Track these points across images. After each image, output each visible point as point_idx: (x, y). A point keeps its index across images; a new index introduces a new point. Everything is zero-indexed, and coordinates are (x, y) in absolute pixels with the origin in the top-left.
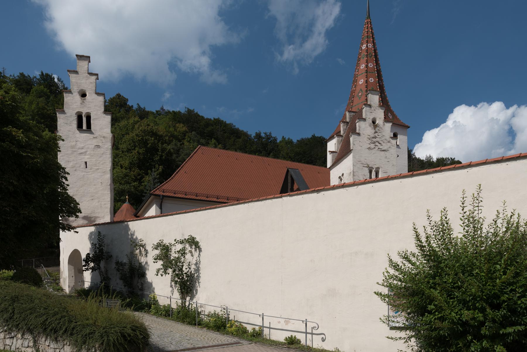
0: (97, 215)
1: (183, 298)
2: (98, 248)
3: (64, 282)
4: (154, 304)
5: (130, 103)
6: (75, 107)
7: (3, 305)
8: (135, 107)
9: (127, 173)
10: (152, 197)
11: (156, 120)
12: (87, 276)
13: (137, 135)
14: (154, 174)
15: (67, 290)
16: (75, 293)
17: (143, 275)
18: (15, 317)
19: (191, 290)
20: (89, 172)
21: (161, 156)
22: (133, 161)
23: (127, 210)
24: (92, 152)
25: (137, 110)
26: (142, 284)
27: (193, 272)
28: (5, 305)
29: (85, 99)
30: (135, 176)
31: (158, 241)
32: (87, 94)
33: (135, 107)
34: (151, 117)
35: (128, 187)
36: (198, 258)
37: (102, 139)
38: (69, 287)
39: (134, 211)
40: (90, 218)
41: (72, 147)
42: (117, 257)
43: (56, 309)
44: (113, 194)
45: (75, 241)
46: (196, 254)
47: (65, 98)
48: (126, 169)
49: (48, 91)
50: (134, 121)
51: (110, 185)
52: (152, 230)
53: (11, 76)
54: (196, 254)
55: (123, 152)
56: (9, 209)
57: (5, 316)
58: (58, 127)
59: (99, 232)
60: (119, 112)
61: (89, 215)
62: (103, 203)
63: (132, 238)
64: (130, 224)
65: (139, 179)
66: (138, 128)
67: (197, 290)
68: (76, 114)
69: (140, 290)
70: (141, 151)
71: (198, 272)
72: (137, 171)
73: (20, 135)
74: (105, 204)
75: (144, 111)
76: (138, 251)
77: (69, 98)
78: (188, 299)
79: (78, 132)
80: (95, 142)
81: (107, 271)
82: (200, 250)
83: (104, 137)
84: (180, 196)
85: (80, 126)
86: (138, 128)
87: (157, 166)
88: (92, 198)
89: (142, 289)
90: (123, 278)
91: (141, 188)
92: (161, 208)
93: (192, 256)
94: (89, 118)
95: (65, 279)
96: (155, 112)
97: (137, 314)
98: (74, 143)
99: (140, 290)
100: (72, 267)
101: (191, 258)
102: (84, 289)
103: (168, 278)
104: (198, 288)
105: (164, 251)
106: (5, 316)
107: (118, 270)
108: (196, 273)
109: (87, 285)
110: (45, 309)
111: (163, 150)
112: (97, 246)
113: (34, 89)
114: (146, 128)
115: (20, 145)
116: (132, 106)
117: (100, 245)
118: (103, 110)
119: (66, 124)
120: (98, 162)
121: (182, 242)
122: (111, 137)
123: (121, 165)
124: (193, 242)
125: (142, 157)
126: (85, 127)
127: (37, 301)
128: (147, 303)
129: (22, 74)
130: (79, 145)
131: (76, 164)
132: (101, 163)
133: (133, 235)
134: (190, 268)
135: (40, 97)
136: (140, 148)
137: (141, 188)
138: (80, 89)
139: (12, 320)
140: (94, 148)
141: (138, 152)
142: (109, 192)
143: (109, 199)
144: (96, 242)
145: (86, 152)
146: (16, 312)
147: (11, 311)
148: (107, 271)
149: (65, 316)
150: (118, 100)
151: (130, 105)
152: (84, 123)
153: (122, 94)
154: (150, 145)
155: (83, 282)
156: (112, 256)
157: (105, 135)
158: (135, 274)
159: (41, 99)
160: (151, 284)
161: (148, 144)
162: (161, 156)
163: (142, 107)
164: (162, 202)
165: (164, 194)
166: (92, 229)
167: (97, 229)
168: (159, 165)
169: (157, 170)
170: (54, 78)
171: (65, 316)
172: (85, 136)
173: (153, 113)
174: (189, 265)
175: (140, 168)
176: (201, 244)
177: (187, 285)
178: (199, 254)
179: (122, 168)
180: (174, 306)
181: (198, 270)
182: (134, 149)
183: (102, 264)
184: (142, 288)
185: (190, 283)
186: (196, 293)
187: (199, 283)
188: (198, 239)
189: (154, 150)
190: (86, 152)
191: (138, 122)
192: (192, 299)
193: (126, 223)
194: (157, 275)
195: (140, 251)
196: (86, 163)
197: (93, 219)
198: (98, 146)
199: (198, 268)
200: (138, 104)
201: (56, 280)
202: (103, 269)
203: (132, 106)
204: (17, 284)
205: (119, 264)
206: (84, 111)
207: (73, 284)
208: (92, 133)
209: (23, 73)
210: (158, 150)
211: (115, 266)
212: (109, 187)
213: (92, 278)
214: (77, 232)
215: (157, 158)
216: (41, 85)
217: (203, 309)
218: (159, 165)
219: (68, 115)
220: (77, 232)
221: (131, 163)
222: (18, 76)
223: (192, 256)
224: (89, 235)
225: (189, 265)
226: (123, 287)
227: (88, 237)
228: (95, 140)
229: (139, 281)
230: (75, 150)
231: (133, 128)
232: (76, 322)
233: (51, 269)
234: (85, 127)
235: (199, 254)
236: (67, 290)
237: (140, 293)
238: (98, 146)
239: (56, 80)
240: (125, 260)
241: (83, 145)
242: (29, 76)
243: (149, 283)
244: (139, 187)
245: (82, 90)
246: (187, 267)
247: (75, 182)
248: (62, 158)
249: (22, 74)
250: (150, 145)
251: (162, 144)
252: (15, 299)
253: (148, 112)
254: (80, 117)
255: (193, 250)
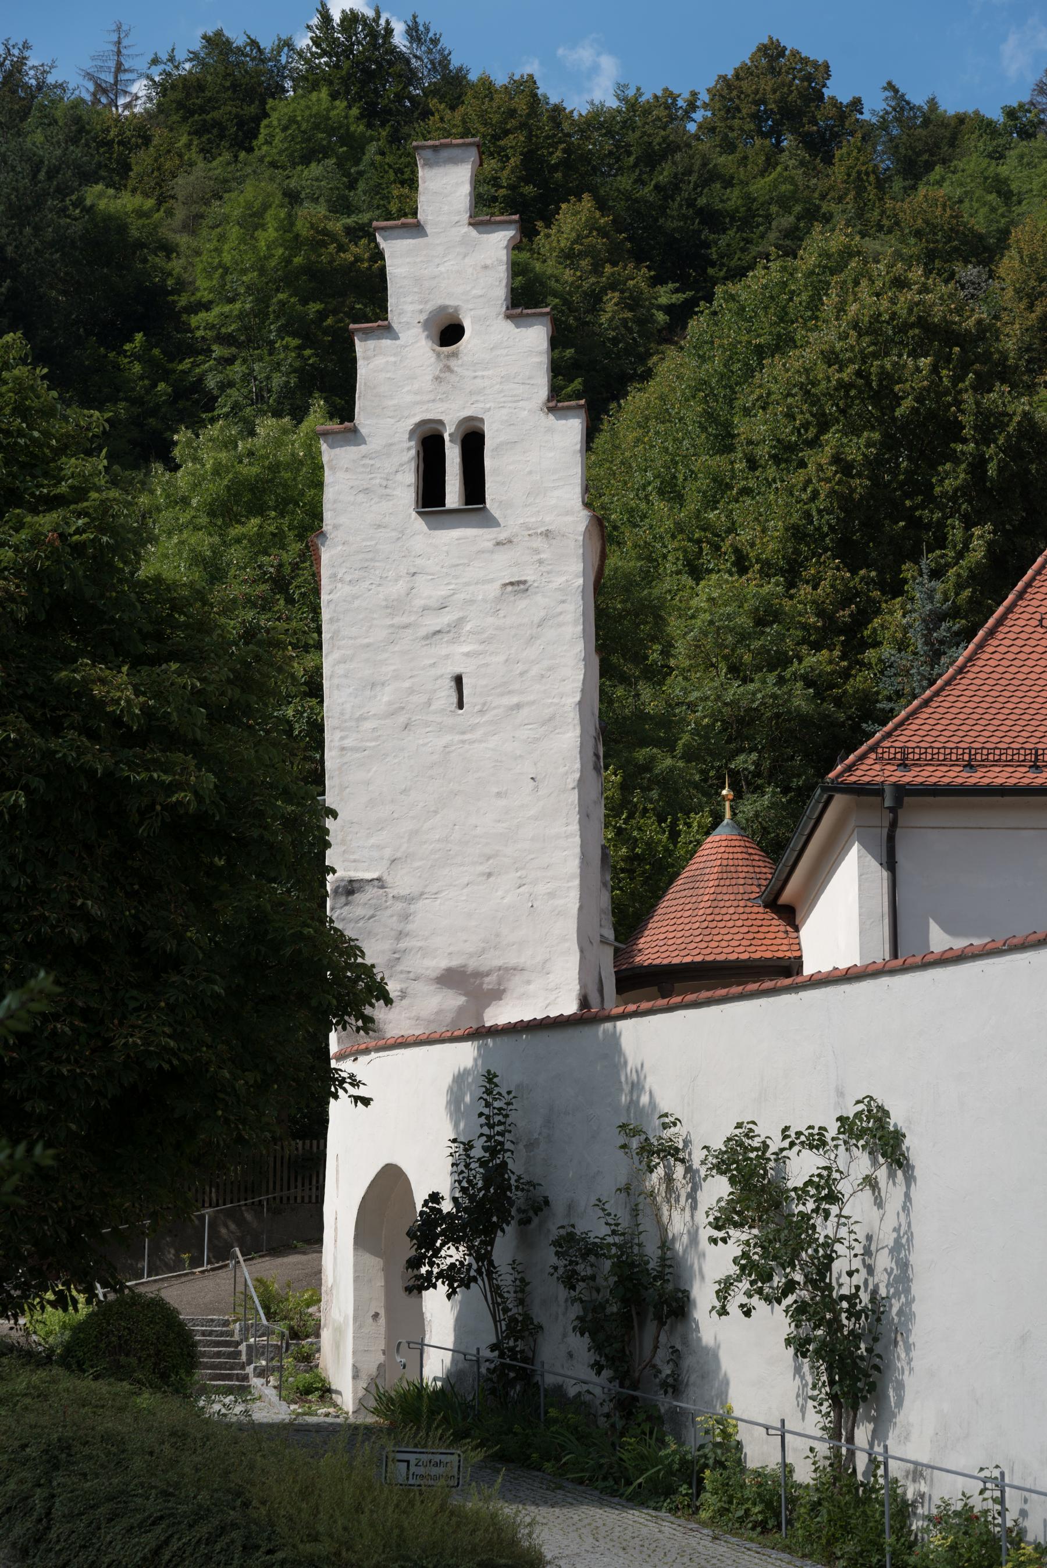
0: (511, 959)
1: (838, 1431)
2: (483, 1163)
3: (337, 1346)
4: (720, 1464)
5: (838, 89)
6: (409, 398)
7: (12, 1485)
8: (875, 105)
9: (766, 601)
10: (839, 801)
11: (1004, 170)
12: (439, 1310)
13: (831, 358)
14: (925, 591)
15: (347, 1394)
16: (376, 1412)
17: (678, 1307)
18: (52, 1535)
19: (872, 1387)
20: (473, 728)
21: (979, 465)
22: (808, 515)
23: (726, 872)
24: (490, 620)
25: (884, 124)
26: (676, 1356)
27: (883, 1292)
28: (21, 1482)
29: (455, 355)
30: (820, 613)
31: (730, 1131)
32: (467, 324)
33: (875, 105)
34: (972, 162)
35: (772, 689)
36: (902, 1215)
37: (538, 543)
38: (355, 1377)
39: (766, 870)
40: (478, 975)
41: (393, 607)
42: (571, 1207)
43: (203, 1497)
44: (600, 835)
45: (393, 1121)
46: (893, 1193)
47: (360, 363)
48: (767, 570)
49: (355, 111)
50: (825, 254)
51: (581, 783)
52: (707, 1072)
53: (155, 61)
54: (893, 1193)
55: (753, 464)
56: (72, 1026)
57: (18, 1530)
58: (327, 515)
59: (490, 1077)
60: (770, 163)
61: (473, 964)
62: (542, 889)
63: (634, 1103)
64: (624, 1027)
65: (848, 630)
66: (841, 309)
67: (900, 1386)
68: (412, 432)
69: (665, 1385)
70: (857, 449)
71: (907, 1291)
72: (830, 575)
73: (119, 688)
74: (552, 895)
75: (927, 122)
76: (660, 1171)
77: (379, 361)
78: (862, 1434)
79: (419, 524)
80: (503, 567)
81: (522, 1285)
82: (910, 1179)
83: (547, 534)
84: (998, 776)
85: (430, 496)
86: (841, 309)
87: (956, 532)
88: (484, 868)
89: (675, 1386)
90: (591, 1324)
91: (860, 681)
92: (890, 864)
93: (879, 1203)
94: (473, 442)
95: (339, 1331)
96: (995, 114)
97: (508, 1510)
98: (398, 588)
99: (665, 1385)
100: (374, 1263)
101: (875, 1213)
102: (420, 1390)
103: (774, 1322)
104: (906, 1377)
105: (752, 1179)
106: (18, 1530)
107: (570, 1280)
108: (897, 1295)
109: (435, 1366)
110: (165, 1494)
111: (989, 424)
112: (477, 1152)
113: (275, 116)
114: (885, 303)
115: (126, 735)
116: (856, 104)
117: (494, 1149)
118: (542, 391)
119: (366, 491)
120: (520, 668)
121: (816, 1141)
122: (582, 527)
123: (737, 551)
124: (877, 1134)
125: (860, 485)
126: (453, 494)
127: (138, 1463)
128: (683, 1462)
129: (216, 43)
130: (428, 592)
131: (411, 691)
132: (535, 671)
133: (637, 1087)
134: (870, 1270)
135: (306, 160)
136: (854, 430)
137: (860, 681)
138: (430, 307)
139: (43, 1546)
140: (499, 599)
141: (836, 459)
142: (575, 827)
143: (573, 865)
144: (474, 1128)
145: (460, 622)
146: (59, 1509)
147: (39, 1508)
148: (522, 1285)
149: (234, 1526)
150: (767, 84)
151: (845, 99)
152: (450, 472)
153: (789, 43)
154: (908, 403)
155: (419, 1346)
156: (547, 1202)
157: (552, 520)
158: (639, 1303)
159: (315, 169)
160: (712, 1355)
161: (898, 400)
162: (979, 465)
163: (918, 98)
164: (893, 825)
165: (908, 777)
166: (464, 1055)
167: (483, 1055)
168: (969, 523)
169: (960, 555)
170: (389, 31)
171: (234, 1526)
172: (457, 538)
173: (987, 127)
174: (867, 1252)
175: (850, 555)
176: (913, 1145)
177: (852, 1358)
178: (907, 1196)
179: (743, 570)
180: (804, 1474)
181: (903, 1277)
182: (814, 443)
183: (504, 1248)
184: (676, 1375)
185: (869, 1350)
186: (900, 1403)
187: (908, 1348)
188: (897, 1119)
189: (931, 434)
190: (460, 622)
191: (848, 253)
192: (879, 1435)
193: (608, 1025)
194: (723, 1312)
195: (669, 1179)
196: (458, 680)
197: (489, 983)
198: (518, 586)
199: (904, 1266)
200: (890, 86)
201: (301, 1334)
202: (506, 1278)
203: (856, 104)
204: (85, 1385)
205: (570, 1243)
206: (450, 416)
207: (375, 1359)
208: (490, 522)
209: (219, 34)
210: (953, 431)
211: (554, 1260)
212: (574, 797)
213: (461, 1326)
214: (366, 1101)
215: (952, 479)
216: (315, 87)
217: (923, 1488)
218: (969, 523)
219: (374, 444)
220: (366, 1101)
221: (797, 533)
222: (194, 57)
223: (879, 1203)
224: (451, 1090)
225: (867, 1252)
226: (590, 1375)
227: (442, 1099)
228: (503, 557)
229: (663, 1338)
230: (404, 620)
231: (814, 304)
232: (270, 1552)
233: (276, 1270)
234: (453, 494)
235: (907, 1196)
236: (347, 1394)
237: (664, 1403)
238: (518, 586)
239: (400, 40)
240: (595, 1228)
241: (443, 591)
242: (254, 43)
243: (706, 1350)
244: (846, 674)
245: (443, 309)
246: (857, 1263)
247: (405, 791)
248: (341, 670)
249: (216, 43)
250: (908, 403)
251: (982, 386)
252: (58, 1456)
253: (961, 119)
254: (430, 445)
255: (882, 1174)
